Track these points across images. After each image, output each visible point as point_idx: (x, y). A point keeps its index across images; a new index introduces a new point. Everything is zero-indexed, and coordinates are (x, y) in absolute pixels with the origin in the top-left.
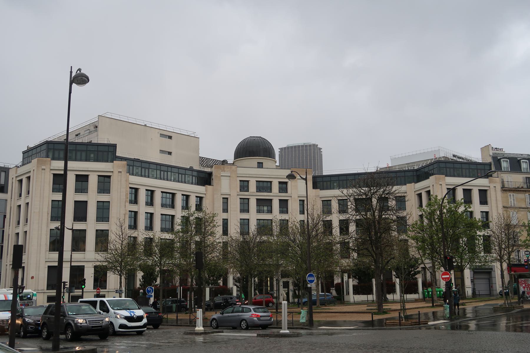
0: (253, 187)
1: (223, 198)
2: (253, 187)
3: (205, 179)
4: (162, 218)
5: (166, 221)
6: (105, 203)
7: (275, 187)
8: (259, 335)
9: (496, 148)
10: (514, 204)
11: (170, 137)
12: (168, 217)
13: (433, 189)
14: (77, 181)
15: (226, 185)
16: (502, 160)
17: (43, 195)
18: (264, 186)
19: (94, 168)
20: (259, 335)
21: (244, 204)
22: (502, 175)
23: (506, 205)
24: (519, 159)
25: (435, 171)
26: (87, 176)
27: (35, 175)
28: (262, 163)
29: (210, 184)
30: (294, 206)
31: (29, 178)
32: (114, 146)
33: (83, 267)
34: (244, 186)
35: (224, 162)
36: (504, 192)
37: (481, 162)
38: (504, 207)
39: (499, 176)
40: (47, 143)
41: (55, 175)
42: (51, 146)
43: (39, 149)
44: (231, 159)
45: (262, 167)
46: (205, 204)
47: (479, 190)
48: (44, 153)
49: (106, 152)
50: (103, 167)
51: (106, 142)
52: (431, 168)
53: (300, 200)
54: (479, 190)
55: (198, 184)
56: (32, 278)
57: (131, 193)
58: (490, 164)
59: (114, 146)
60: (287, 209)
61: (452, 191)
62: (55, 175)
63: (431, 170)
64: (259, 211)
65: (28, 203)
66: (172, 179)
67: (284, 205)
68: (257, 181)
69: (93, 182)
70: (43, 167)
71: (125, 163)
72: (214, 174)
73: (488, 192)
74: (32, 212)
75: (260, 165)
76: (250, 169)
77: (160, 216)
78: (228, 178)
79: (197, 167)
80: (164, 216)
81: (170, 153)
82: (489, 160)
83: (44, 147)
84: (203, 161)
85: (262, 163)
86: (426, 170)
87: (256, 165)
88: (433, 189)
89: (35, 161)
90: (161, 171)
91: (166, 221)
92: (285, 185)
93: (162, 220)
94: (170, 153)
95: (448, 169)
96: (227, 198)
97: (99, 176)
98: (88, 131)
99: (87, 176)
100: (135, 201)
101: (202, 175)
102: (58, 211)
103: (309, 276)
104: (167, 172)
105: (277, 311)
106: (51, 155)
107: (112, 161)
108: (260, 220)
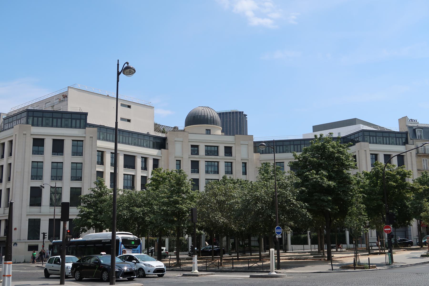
0: (202, 151)
1: (177, 160)
2: (202, 151)
3: (161, 144)
4: (124, 177)
5: (127, 180)
6: (39, 164)
7: (222, 151)
8: (251, 277)
9: (411, 120)
10: (427, 167)
11: (129, 107)
12: (129, 176)
13: (359, 154)
14: (34, 145)
15: (178, 150)
16: (417, 130)
17: (22, 158)
18: (212, 151)
19: (68, 134)
20: (251, 277)
21: (208, 166)
22: (417, 143)
23: (420, 168)
24: (414, 128)
25: (360, 139)
26: (43, 139)
27: (17, 139)
28: (210, 130)
29: (164, 148)
30: (238, 169)
31: (11, 142)
32: (86, 114)
33: (39, 220)
34: (195, 149)
35: (175, 129)
36: (419, 157)
37: (398, 131)
38: (418, 170)
39: (414, 143)
40: (28, 111)
41: (34, 139)
42: (31, 114)
43: (19, 117)
44: (181, 126)
45: (210, 134)
46: (161, 165)
47: (384, 155)
48: (24, 120)
49: (79, 119)
50: (76, 133)
51: (78, 111)
52: (356, 135)
53: (243, 163)
54: (384, 155)
55: (154, 147)
56: (15, 229)
57: (98, 156)
58: (406, 133)
59: (86, 114)
60: (198, 169)
61: (375, 157)
62: (34, 139)
63: (356, 138)
64: (207, 172)
65: (10, 164)
66: (145, 145)
67: (229, 166)
68: (206, 146)
69: (48, 146)
70: (25, 133)
71: (96, 129)
72: (168, 138)
73: (405, 158)
74: (15, 171)
75: (208, 132)
76: (199, 135)
77: (123, 176)
78: (246, 146)
79: (153, 133)
80: (126, 176)
81: (129, 121)
82: (406, 129)
83: (361, 134)
84: (157, 127)
85: (210, 130)
86: (352, 137)
87: (205, 132)
88: (359, 154)
89: (17, 127)
90: (294, 145)
91: (127, 180)
92: (197, 149)
93: (124, 179)
94: (129, 121)
95: (398, 139)
96: (180, 161)
97: (73, 140)
98: (58, 100)
99: (43, 139)
100: (101, 162)
101: (158, 141)
102: (37, 172)
103: (277, 228)
104: (301, 145)
105: (238, 257)
106: (30, 121)
107: (84, 128)
108: (208, 179)
